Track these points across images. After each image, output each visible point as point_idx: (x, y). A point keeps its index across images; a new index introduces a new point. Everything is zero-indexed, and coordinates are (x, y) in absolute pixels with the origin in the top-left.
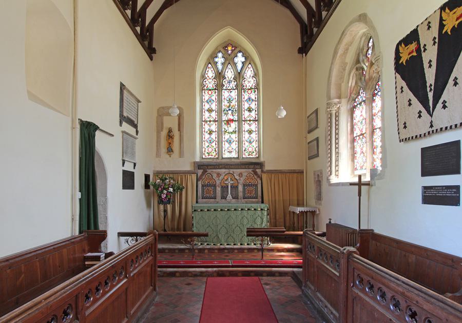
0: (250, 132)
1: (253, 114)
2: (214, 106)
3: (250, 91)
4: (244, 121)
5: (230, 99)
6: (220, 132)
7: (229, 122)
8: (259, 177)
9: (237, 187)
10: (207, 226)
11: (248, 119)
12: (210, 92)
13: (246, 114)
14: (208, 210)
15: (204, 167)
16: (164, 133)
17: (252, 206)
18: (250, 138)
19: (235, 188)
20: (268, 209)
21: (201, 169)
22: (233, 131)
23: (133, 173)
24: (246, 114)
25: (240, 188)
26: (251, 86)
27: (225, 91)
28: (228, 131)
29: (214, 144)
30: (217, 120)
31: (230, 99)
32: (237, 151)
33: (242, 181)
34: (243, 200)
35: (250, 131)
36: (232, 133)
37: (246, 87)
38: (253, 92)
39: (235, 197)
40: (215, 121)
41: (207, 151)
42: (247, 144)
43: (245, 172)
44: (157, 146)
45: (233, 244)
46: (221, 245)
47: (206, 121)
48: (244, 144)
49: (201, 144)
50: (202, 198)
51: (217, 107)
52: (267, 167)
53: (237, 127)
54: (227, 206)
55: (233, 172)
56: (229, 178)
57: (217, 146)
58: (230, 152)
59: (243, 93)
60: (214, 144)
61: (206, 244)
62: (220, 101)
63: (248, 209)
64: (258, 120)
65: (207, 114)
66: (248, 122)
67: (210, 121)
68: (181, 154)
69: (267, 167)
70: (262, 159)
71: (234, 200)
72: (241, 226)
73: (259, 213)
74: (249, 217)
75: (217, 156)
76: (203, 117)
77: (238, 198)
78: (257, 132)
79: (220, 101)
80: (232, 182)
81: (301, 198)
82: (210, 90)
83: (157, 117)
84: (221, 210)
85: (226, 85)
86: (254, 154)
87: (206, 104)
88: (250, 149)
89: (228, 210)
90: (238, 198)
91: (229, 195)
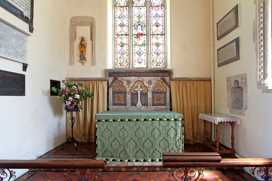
0: (158, 45)
1: (160, 29)
2: (125, 22)
3: (157, 8)
4: (152, 35)
5: (139, 15)
6: (131, 45)
7: (139, 35)
8: (167, 84)
9: (146, 94)
10: (112, 139)
11: (156, 33)
12: (122, 9)
13: (154, 28)
14: (114, 120)
15: (114, 74)
16: (77, 42)
17: (164, 116)
18: (157, 50)
19: (144, 95)
20: (182, 120)
21: (112, 76)
22: (143, 44)
23: (23, 77)
24: (154, 28)
25: (150, 95)
26: (158, 4)
27: (135, 8)
28: (137, 44)
29: (125, 56)
30: (128, 34)
31: (139, 15)
32: (146, 61)
33: (151, 88)
34: (152, 107)
35: (158, 44)
36: (141, 45)
37: (154, 4)
38: (160, 9)
39: (145, 104)
40: (126, 35)
41: (119, 62)
42: (155, 55)
43: (154, 80)
44: (70, 58)
45: (142, 160)
46: (129, 161)
47: (118, 35)
48: (153, 56)
49: (114, 55)
50: (113, 105)
51: (128, 22)
52: (175, 75)
53: (146, 40)
54: (136, 116)
55: (143, 79)
56: (139, 86)
57: (128, 57)
58: (139, 64)
59: (151, 10)
60: (125, 56)
61: (111, 160)
62: (130, 17)
63: (160, 120)
64: (164, 34)
65: (119, 29)
66: (156, 36)
67: (122, 35)
68: (93, 63)
69: (175, 75)
70: (169, 67)
71: (143, 107)
72: (152, 139)
73: (172, 123)
74: (161, 128)
75: (128, 67)
76: (116, 31)
77: (147, 105)
78: (164, 45)
79: (130, 17)
80: (142, 89)
81: (208, 105)
82: (122, 7)
83: (70, 27)
84: (129, 120)
85: (135, 3)
86: (161, 64)
87: (118, 19)
88: (158, 60)
89: (137, 120)
90: (147, 105)
91: (139, 102)
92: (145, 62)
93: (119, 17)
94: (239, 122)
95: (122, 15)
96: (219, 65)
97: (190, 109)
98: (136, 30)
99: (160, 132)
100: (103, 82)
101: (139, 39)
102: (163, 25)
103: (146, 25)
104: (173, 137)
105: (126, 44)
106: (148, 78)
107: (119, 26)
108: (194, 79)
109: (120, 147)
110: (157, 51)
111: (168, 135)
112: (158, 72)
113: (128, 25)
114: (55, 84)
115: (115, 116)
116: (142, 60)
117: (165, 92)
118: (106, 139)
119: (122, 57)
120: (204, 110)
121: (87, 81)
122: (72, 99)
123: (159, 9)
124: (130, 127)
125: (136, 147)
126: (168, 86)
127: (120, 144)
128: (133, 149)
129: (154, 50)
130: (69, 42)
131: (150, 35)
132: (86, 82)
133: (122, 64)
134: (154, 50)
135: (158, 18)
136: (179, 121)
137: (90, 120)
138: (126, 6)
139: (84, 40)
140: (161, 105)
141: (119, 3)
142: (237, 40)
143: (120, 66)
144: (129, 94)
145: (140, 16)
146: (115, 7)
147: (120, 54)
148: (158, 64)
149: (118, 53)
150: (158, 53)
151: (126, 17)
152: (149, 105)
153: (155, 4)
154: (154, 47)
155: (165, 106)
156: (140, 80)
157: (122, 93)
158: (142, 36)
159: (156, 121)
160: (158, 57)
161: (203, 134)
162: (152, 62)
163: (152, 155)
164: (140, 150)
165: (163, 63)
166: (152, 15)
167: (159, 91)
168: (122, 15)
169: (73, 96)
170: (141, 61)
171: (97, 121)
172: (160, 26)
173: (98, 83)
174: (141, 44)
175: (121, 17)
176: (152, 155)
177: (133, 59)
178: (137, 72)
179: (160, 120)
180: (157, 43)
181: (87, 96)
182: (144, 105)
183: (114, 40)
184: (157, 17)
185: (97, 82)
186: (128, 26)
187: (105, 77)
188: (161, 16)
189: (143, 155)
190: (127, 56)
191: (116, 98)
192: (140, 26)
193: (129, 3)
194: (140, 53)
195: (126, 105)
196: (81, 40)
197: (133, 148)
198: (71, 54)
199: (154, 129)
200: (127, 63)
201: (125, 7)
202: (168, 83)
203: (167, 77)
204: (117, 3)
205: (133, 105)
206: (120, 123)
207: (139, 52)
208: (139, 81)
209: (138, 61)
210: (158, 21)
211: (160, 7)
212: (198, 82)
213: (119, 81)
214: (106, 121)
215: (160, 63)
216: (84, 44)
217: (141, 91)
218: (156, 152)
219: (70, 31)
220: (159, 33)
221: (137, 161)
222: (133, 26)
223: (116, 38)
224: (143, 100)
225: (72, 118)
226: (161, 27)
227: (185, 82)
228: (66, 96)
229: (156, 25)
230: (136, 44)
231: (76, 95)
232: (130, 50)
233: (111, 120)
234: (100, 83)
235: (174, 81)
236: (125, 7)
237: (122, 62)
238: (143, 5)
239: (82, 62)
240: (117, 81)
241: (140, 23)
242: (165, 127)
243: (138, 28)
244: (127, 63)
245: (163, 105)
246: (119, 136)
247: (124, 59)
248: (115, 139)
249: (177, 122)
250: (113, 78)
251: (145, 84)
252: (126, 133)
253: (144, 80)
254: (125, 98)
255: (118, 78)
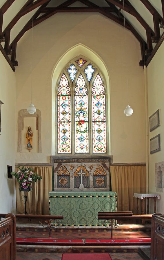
0: (99, 131)
2: (67, 110)
3: (98, 97)
4: (94, 122)
5: (81, 103)
6: (73, 132)
7: (81, 122)
8: (107, 169)
9: (88, 178)
10: (61, 210)
11: (98, 120)
12: (64, 98)
13: (96, 116)
14: (63, 197)
16: (24, 131)
17: (102, 194)
18: (99, 136)
19: (86, 178)
20: (116, 196)
22: (85, 130)
24: (96, 116)
25: (91, 178)
26: (99, 93)
27: (77, 97)
28: (80, 131)
29: (67, 142)
30: (70, 121)
31: (81, 103)
32: (88, 147)
33: (92, 172)
35: (99, 131)
36: (83, 132)
37: (95, 93)
38: (101, 97)
39: (87, 186)
40: (68, 122)
42: (96, 141)
43: (95, 165)
44: (19, 145)
46: (75, 225)
47: (60, 122)
48: (94, 141)
49: (56, 141)
50: (58, 187)
52: (114, 161)
54: (80, 194)
55: (85, 165)
56: (81, 171)
57: (70, 143)
59: (93, 98)
60: (67, 142)
61: (61, 225)
62: (72, 105)
63: (99, 196)
64: (106, 121)
65: (61, 116)
66: (98, 123)
67: (64, 122)
68: (39, 150)
69: (114, 161)
70: (110, 154)
71: (86, 189)
73: (108, 199)
74: (99, 203)
75: (70, 152)
76: (58, 118)
77: (89, 187)
78: (105, 131)
79: (72, 105)
80: (84, 173)
81: (143, 187)
82: (64, 96)
84: (75, 197)
85: (78, 92)
86: (103, 150)
87: (61, 107)
88: (99, 146)
89: (81, 197)
90: (89, 187)
91: (82, 184)
92: (87, 147)
93: (61, 105)
94: (159, 197)
95: (64, 103)
96: (152, 153)
97: (127, 189)
98: (77, 117)
99: (99, 205)
100: (49, 167)
101: (81, 126)
102: (105, 112)
103: (87, 112)
104: (109, 209)
105: (68, 130)
106: (90, 164)
107: (62, 113)
108: (131, 164)
109: (67, 216)
110: (99, 137)
111: (105, 208)
112: (99, 158)
113: (70, 113)
114: (10, 168)
115: (64, 194)
116: (84, 145)
117: (105, 176)
118: (57, 210)
119: (64, 143)
120: (139, 190)
121: (34, 166)
122: (26, 181)
123: (100, 97)
124: (76, 202)
125: (80, 216)
126: (108, 171)
127: (67, 214)
128: (78, 218)
129: (96, 136)
130: (17, 131)
131: (92, 122)
132: (34, 167)
133: (65, 150)
134: (96, 136)
135: (100, 106)
136: (113, 197)
137: (37, 200)
138: (69, 95)
139: (31, 130)
140: (102, 187)
141: (62, 93)
142: (159, 136)
143: (63, 151)
144: (72, 177)
145: (82, 104)
146: (58, 96)
147: (62, 139)
148: (100, 150)
149: (60, 139)
150: (100, 139)
151: (68, 105)
152: (90, 187)
153: (96, 93)
154: (96, 134)
155: (106, 188)
156: (82, 165)
157: (66, 177)
158: (84, 123)
159: (95, 198)
160: (100, 143)
161: (137, 209)
162: (94, 147)
163: (92, 222)
164: (83, 218)
165: (105, 148)
166: (94, 103)
167: (100, 175)
168: (64, 103)
169: (27, 179)
170: (84, 147)
171: (50, 197)
172: (102, 114)
173: (44, 168)
174: (83, 131)
175: (63, 105)
176: (92, 222)
177: (76, 144)
178: (80, 159)
179: (99, 196)
180: (99, 129)
181: (37, 179)
182: (86, 187)
183: (56, 127)
184: (99, 105)
185: (43, 167)
186: (70, 114)
187: (51, 163)
188: (103, 104)
189: (85, 222)
190: (69, 142)
191: (61, 181)
192: (82, 113)
193: (71, 92)
194: (82, 139)
195: (69, 187)
196: (28, 130)
197: (78, 217)
198: (19, 143)
199: (94, 203)
200: (70, 149)
201: (67, 96)
202: (108, 168)
203: (107, 162)
204: (60, 93)
205: (76, 187)
206: (68, 199)
207: (81, 138)
208: (82, 166)
209: (80, 147)
210: (99, 109)
211: (102, 96)
212: (135, 166)
213: (63, 166)
214: (57, 197)
215: (102, 148)
216: (31, 134)
217: (83, 175)
218: (96, 220)
219: (18, 122)
220: (100, 120)
221: (80, 225)
222: (75, 114)
223: (58, 125)
224: (85, 183)
225: (26, 197)
226: (102, 114)
227: (123, 166)
228: (22, 178)
229: (97, 112)
230: (78, 131)
231: (29, 178)
232: (72, 136)
233: (60, 197)
234: (46, 168)
235: (114, 166)
236: (67, 96)
237: (64, 147)
238: (85, 94)
239: (29, 149)
240: (61, 166)
241: (82, 111)
242: (103, 201)
243: (80, 116)
244: (70, 149)
245: (104, 187)
246: (67, 208)
247: (67, 145)
248: (64, 210)
249: (112, 198)
250: (57, 163)
251: (87, 169)
252: (73, 206)
253: (86, 165)
254: (69, 181)
255: (62, 163)
